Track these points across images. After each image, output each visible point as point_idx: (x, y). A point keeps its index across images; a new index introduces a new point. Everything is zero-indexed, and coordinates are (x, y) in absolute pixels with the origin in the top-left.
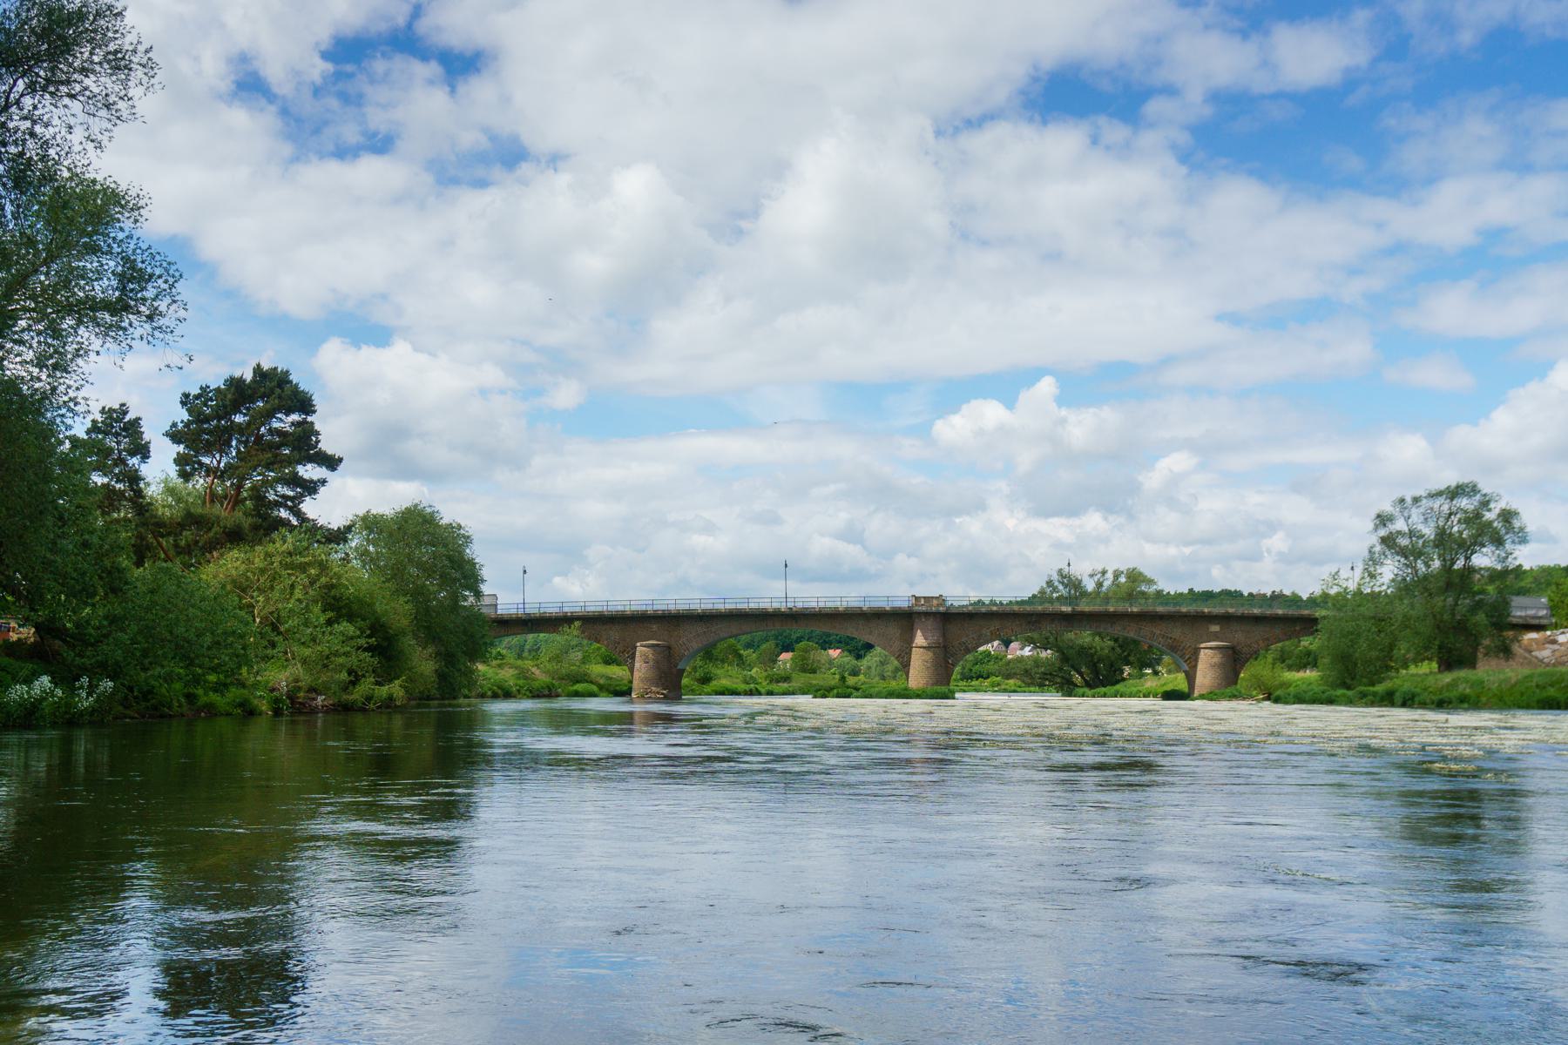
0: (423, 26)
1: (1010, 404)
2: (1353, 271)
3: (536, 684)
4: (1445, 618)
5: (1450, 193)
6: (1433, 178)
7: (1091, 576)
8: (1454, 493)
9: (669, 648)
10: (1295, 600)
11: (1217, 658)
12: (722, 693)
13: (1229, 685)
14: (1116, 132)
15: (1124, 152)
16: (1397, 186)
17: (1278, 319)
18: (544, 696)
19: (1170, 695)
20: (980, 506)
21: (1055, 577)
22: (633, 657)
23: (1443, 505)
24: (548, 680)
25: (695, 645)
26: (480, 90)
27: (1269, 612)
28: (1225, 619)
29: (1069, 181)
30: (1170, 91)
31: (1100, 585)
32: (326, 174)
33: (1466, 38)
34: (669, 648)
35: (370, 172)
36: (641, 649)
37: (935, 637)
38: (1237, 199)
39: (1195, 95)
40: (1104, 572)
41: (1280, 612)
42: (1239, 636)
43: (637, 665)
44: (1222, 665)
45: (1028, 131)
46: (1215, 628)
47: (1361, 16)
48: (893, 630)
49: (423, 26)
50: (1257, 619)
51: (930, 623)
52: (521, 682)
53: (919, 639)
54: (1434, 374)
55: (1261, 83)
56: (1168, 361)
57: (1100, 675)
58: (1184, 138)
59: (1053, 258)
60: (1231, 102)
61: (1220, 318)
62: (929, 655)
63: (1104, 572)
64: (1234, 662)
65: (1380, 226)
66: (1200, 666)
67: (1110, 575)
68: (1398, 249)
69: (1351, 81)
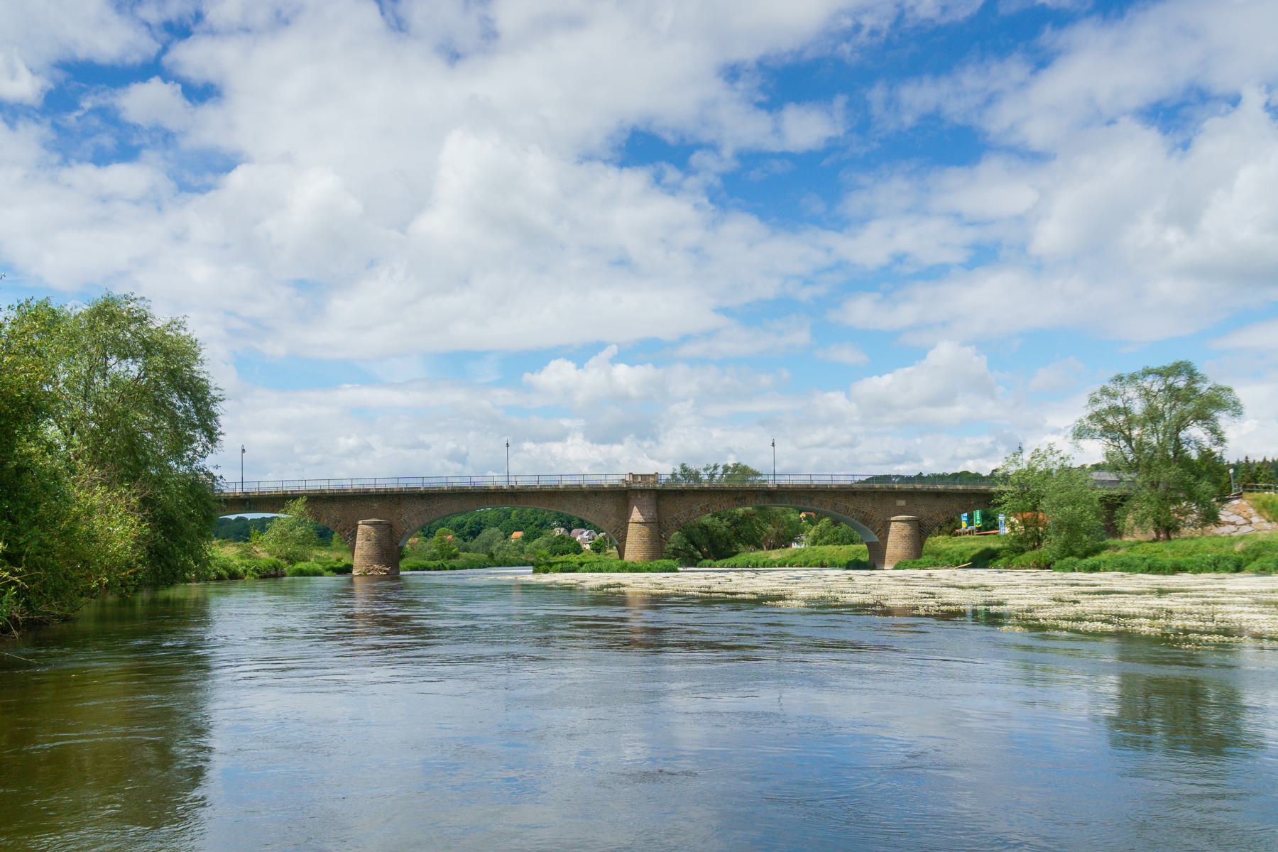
0: (167, 60)
1: (580, 365)
2: (807, 282)
3: (262, 564)
4: (1167, 487)
5: (875, 231)
6: (864, 220)
7: (705, 470)
8: (1177, 369)
9: (390, 526)
10: (977, 477)
11: (907, 530)
12: (416, 569)
13: (917, 555)
14: (672, 175)
15: (673, 190)
16: (840, 224)
17: (755, 315)
18: (271, 576)
19: (856, 565)
20: (561, 437)
21: (679, 470)
22: (354, 535)
23: (1156, 385)
24: (273, 559)
25: (416, 523)
26: (209, 113)
27: (951, 487)
28: (911, 495)
29: (638, 210)
30: (713, 147)
31: (712, 476)
32: (84, 175)
33: (909, 120)
34: (390, 526)
35: (121, 177)
36: (363, 528)
37: (651, 513)
38: (741, 228)
39: (727, 152)
40: (716, 467)
41: (960, 487)
42: (934, 511)
43: (359, 543)
44: (912, 536)
45: (612, 172)
46: (901, 503)
47: (840, 101)
48: (610, 507)
49: (167, 60)
50: (938, 495)
51: (646, 499)
52: (246, 561)
53: (636, 515)
54: (846, 355)
55: (772, 145)
56: (686, 339)
57: (712, 548)
58: (717, 183)
59: (622, 264)
60: (751, 158)
61: (715, 311)
62: (645, 530)
63: (716, 467)
64: (921, 532)
65: (829, 250)
66: (891, 537)
67: (720, 470)
68: (840, 266)
69: (832, 146)
